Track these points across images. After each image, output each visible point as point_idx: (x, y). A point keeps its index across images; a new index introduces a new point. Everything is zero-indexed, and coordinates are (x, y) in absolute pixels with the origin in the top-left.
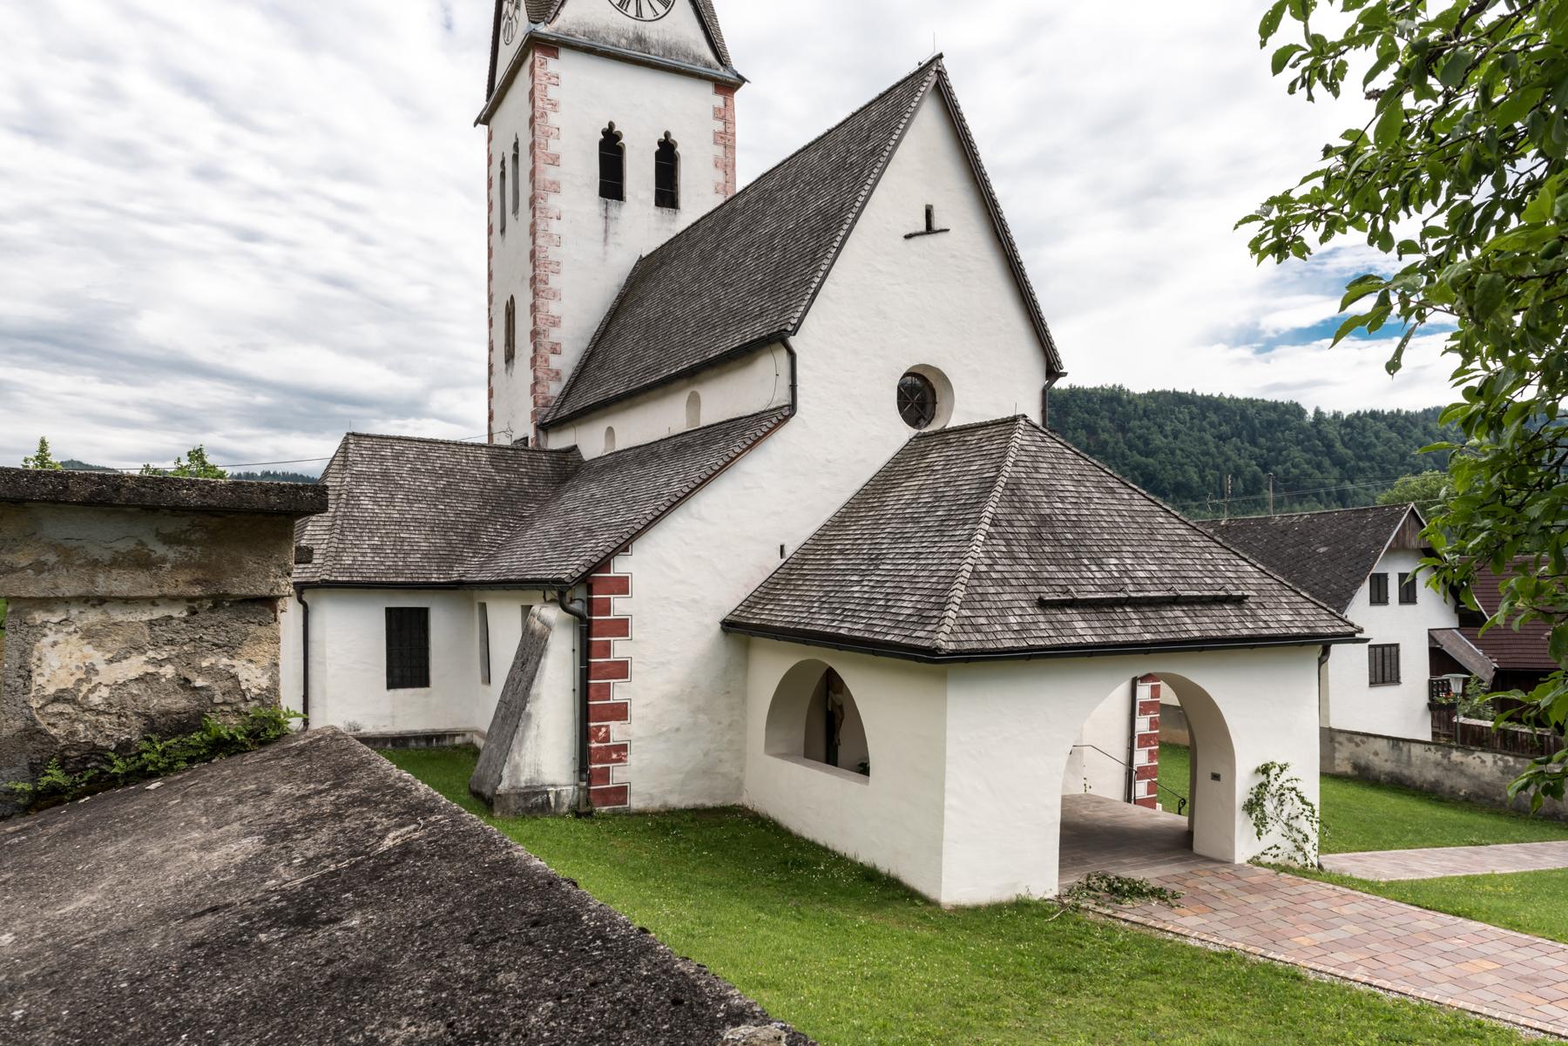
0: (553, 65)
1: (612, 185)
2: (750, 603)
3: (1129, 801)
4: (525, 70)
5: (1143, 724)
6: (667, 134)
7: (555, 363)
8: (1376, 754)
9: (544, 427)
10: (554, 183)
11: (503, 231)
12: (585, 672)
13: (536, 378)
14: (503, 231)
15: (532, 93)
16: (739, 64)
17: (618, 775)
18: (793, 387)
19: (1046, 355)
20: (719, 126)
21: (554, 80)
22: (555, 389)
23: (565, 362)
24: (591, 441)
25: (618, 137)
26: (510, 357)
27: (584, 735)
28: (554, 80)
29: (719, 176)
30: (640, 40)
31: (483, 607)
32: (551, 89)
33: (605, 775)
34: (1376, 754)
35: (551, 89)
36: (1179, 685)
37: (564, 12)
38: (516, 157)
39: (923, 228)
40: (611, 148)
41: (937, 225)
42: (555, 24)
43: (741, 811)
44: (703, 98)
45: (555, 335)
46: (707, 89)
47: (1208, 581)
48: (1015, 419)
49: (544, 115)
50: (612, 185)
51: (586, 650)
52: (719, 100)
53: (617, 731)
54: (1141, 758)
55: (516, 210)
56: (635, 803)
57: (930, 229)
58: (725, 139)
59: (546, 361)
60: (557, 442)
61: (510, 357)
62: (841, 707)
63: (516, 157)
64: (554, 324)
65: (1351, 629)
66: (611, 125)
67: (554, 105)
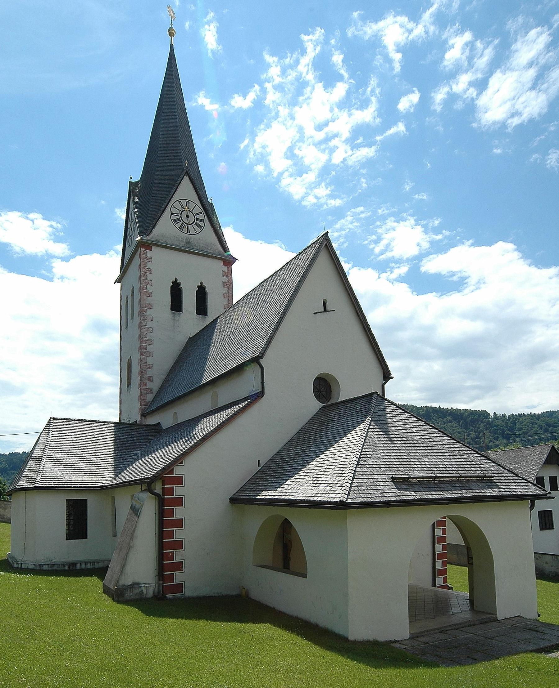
0: (149, 253)
1: (176, 305)
2: (242, 489)
3: (435, 586)
4: (137, 256)
5: (439, 548)
6: (201, 283)
7: (150, 385)
8: (547, 563)
9: (144, 415)
10: (150, 304)
11: (127, 327)
12: (161, 524)
13: (141, 393)
14: (127, 327)
15: (140, 266)
16: (233, 252)
17: (178, 577)
18: (263, 383)
19: (383, 368)
20: (225, 279)
21: (150, 260)
22: (150, 397)
23: (155, 385)
24: (166, 419)
25: (179, 284)
26: (129, 384)
27: (161, 557)
28: (150, 260)
29: (226, 301)
30: (188, 243)
31: (113, 498)
32: (148, 263)
33: (171, 577)
34: (547, 563)
35: (148, 263)
36: (463, 526)
37: (154, 231)
38: (133, 295)
39: (323, 310)
40: (176, 291)
41: (328, 309)
42: (151, 236)
43: (330, 387)
44: (218, 265)
45: (150, 373)
46: (220, 263)
47: (474, 469)
48: (372, 394)
49: (145, 275)
50: (176, 305)
51: (162, 513)
52: (225, 268)
53: (178, 556)
54: (439, 565)
55: (132, 318)
56: (188, 592)
57: (325, 310)
58: (229, 285)
59: (146, 385)
60: (151, 421)
61: (129, 384)
62: (290, 541)
63: (133, 295)
64: (150, 368)
65: (544, 493)
66: (176, 279)
67: (150, 271)
